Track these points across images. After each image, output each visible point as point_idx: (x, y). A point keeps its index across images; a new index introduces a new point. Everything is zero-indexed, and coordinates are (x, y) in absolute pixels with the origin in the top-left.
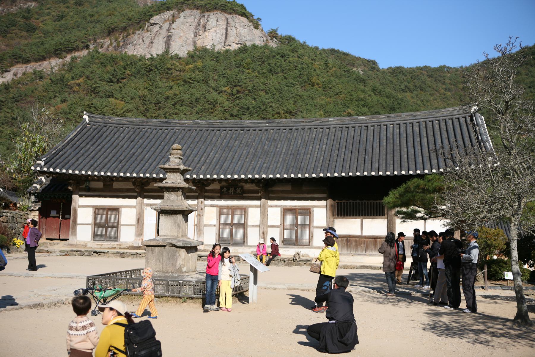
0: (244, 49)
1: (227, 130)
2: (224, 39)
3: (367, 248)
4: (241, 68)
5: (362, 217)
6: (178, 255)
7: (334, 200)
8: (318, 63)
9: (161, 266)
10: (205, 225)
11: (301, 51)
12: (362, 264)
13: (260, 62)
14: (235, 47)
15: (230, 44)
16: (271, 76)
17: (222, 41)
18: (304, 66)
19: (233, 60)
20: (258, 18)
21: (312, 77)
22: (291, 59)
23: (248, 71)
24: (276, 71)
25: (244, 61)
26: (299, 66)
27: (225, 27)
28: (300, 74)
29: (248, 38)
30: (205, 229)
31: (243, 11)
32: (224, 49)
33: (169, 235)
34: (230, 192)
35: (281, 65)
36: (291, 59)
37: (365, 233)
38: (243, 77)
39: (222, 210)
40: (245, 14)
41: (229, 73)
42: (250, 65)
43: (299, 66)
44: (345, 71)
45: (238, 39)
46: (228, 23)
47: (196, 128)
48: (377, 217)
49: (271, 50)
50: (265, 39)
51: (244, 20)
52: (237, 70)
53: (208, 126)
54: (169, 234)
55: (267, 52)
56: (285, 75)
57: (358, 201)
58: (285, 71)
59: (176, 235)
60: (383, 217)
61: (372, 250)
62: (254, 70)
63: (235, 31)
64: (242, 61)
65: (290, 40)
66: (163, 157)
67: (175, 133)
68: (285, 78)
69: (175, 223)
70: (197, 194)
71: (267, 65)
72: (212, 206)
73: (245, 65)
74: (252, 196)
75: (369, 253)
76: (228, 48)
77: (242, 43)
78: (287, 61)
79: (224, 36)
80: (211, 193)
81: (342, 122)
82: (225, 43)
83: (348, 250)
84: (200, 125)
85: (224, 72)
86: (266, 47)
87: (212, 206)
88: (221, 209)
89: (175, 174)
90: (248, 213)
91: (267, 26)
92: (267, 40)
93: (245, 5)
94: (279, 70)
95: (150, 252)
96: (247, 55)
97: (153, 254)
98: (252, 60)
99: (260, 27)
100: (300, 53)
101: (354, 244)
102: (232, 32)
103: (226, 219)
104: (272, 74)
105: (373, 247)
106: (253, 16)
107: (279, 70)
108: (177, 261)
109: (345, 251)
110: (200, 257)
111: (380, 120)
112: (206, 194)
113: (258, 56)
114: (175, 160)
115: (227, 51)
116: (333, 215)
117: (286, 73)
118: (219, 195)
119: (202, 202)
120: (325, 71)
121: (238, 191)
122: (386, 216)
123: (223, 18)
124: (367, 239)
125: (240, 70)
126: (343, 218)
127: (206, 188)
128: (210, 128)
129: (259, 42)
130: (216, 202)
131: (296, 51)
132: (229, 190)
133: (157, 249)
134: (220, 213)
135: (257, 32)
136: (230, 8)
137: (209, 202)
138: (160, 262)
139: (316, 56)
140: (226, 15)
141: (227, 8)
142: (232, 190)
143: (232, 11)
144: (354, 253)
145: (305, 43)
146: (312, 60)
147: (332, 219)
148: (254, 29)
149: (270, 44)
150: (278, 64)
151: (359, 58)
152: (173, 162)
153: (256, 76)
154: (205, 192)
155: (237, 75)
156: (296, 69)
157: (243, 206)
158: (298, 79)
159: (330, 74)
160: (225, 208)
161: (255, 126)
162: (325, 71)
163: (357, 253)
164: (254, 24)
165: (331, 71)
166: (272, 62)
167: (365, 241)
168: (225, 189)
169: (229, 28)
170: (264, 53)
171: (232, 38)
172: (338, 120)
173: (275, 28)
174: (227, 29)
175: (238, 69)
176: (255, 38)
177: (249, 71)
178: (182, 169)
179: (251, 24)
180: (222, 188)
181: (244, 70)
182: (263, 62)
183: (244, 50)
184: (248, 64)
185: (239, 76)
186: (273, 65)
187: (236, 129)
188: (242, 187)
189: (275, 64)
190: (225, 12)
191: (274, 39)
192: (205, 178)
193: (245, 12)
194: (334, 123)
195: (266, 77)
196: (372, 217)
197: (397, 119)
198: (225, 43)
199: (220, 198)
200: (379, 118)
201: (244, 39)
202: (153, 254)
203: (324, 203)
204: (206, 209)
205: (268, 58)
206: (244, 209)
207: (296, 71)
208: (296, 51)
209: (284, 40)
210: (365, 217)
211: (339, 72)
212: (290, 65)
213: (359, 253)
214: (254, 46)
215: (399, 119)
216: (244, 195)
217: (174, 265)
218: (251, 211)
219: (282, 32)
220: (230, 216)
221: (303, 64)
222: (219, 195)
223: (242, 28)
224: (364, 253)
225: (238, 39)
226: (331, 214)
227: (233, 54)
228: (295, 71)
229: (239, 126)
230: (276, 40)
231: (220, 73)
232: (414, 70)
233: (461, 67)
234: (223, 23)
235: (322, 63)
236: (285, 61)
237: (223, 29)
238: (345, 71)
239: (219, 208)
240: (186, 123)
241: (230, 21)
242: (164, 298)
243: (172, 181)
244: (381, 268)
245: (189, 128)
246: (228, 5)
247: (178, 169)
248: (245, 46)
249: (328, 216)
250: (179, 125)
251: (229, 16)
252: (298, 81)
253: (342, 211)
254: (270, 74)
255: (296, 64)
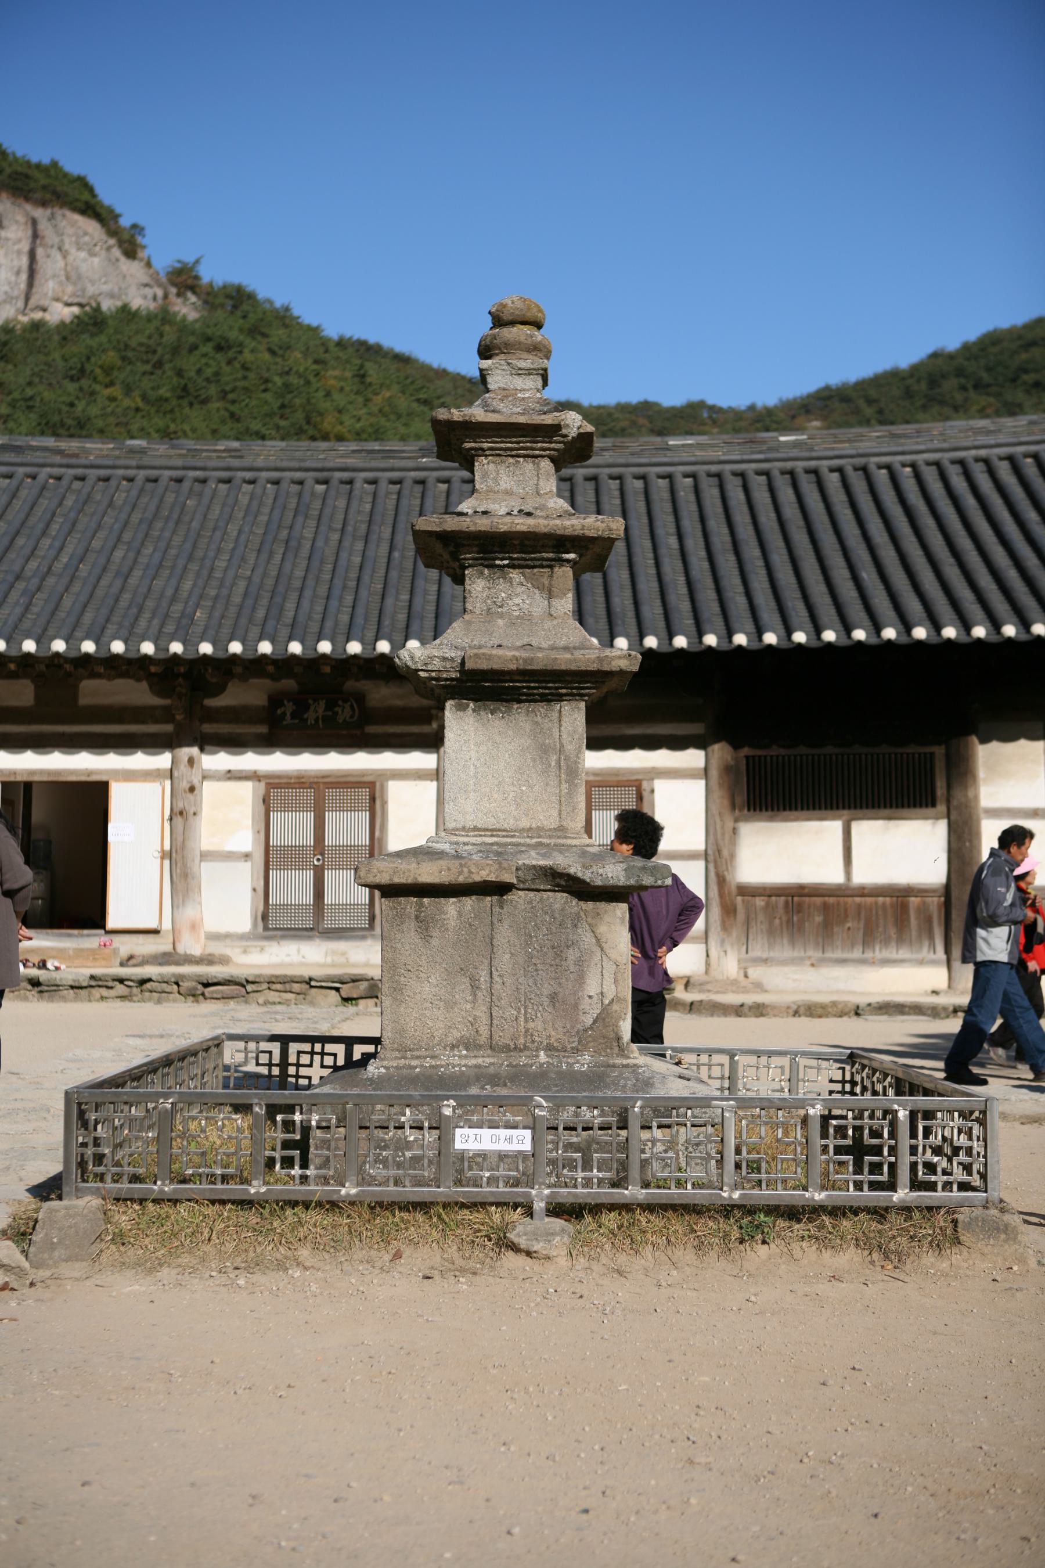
0: (92, 321)
1: (261, 482)
2: (23, 286)
3: (869, 936)
4: (85, 383)
5: (846, 813)
6: (588, 939)
7: (736, 746)
8: (337, 373)
9: (481, 1012)
10: (205, 856)
11: (278, 335)
12: (880, 999)
13: (147, 362)
14: (60, 313)
15: (45, 302)
16: (187, 410)
17: (16, 293)
18: (294, 380)
19: (57, 355)
20: (134, 226)
21: (321, 414)
22: (247, 356)
23: (107, 392)
24: (203, 394)
25: (93, 360)
26: (278, 380)
27: (25, 246)
28: (283, 406)
29: (105, 288)
30: (207, 872)
31: (86, 196)
32: (24, 319)
33: (510, 823)
34: (310, 716)
35: (217, 374)
36: (247, 356)
37: (864, 875)
38: (94, 411)
39: (275, 792)
40: (91, 208)
41: (47, 395)
42: (115, 373)
43: (278, 380)
44: (418, 400)
45: (70, 289)
46: (35, 236)
47: (131, 473)
48: (905, 812)
49: (183, 327)
50: (160, 293)
51: (92, 227)
52: (71, 387)
53: (179, 463)
54: (509, 816)
55: (170, 335)
56: (232, 408)
57: (829, 750)
58: (231, 396)
59: (552, 823)
60: (930, 811)
61: (886, 942)
62: (128, 390)
63: (61, 263)
64: (88, 358)
65: (238, 298)
66: (18, 577)
67: (44, 488)
68: (232, 415)
69: (544, 750)
70: (169, 728)
71: (170, 373)
72: (231, 776)
73: (98, 371)
74: (401, 735)
75: (879, 953)
76: (38, 315)
77: (83, 301)
78: (237, 365)
79: (24, 276)
80: (229, 721)
81: (719, 454)
82: (27, 299)
83: (793, 942)
84: (146, 461)
85: (29, 392)
86: (164, 316)
87: (231, 776)
88: (270, 786)
89: (528, 466)
90: (384, 803)
91: (164, 251)
92: (166, 296)
93: (92, 180)
94: (213, 390)
95: (411, 925)
96: (103, 338)
97: (426, 937)
98: (124, 359)
99: (142, 254)
100: (275, 339)
101: (818, 919)
102: (51, 264)
103: (294, 827)
104: (191, 405)
105: (892, 931)
106: (116, 217)
107: (213, 390)
108: (581, 978)
109: (784, 950)
110: (206, 985)
111: (865, 446)
112: (208, 728)
113: (141, 344)
114: (519, 382)
115: (37, 326)
116: (733, 806)
117: (233, 402)
118: (263, 729)
119: (191, 761)
120: (360, 399)
121: (344, 712)
122: (941, 808)
123: (21, 218)
124: (869, 900)
125: (81, 389)
126: (771, 819)
127: (209, 702)
128: (192, 474)
129: (139, 300)
130: (251, 761)
131: (265, 335)
132: (307, 708)
133: (451, 907)
134: (267, 804)
135: (134, 269)
136: (44, 187)
137: (220, 760)
138: (475, 987)
139: (326, 351)
140: (28, 207)
141: (32, 185)
142: (317, 710)
143: (48, 196)
144: (819, 954)
145: (287, 309)
146: (316, 362)
147: (730, 824)
148: (123, 259)
149: (176, 309)
150: (209, 372)
151: (442, 373)
152: (507, 394)
153: (137, 410)
154: (203, 720)
155: (72, 405)
156: (265, 390)
157: (364, 773)
158: (277, 419)
159: (375, 409)
160: (288, 785)
161: (374, 464)
162: (360, 399)
163: (829, 954)
164: (120, 243)
165: (378, 400)
166: (190, 364)
167: (859, 906)
168: (289, 708)
169: (40, 252)
170: (161, 336)
171: (51, 284)
172: (700, 446)
173: (190, 259)
174: (32, 255)
175: (76, 385)
176: (127, 287)
177: (116, 391)
178: (573, 433)
179: (112, 241)
180: (275, 700)
181: (97, 387)
182: (159, 365)
183: (95, 324)
184: (108, 370)
185: (80, 406)
186: (192, 374)
187: (298, 475)
188: (360, 698)
189: (199, 372)
190: (27, 199)
191: (189, 294)
192: (221, 655)
193: (93, 201)
194: (685, 457)
195: (172, 411)
196: (887, 812)
197: (930, 446)
198: (27, 299)
199: (267, 743)
200: (860, 438)
201: (91, 290)
202: (426, 937)
203: (694, 758)
204: (209, 790)
205: (175, 351)
206: (371, 786)
207: (268, 396)
208: (265, 335)
209: (221, 300)
210: (859, 812)
211: (403, 403)
212: (245, 378)
213: (839, 954)
214: (126, 313)
215: (936, 444)
216: (371, 729)
217: (563, 1003)
218: (396, 792)
219: (214, 273)
220: (311, 816)
221: (288, 373)
222: (263, 729)
223: (83, 254)
224: (857, 953)
225: (70, 289)
226: (726, 802)
227: (56, 338)
228: (263, 395)
229: (308, 464)
230: (193, 298)
231: (16, 395)
232: (610, 415)
233: (752, 408)
234: (20, 234)
235: (348, 374)
236: (229, 362)
237: (19, 252)
238: (418, 400)
239: (262, 786)
240: (88, 452)
241: (44, 226)
242: (610, 1220)
243: (516, 505)
244: (955, 1011)
245: (103, 472)
246: (37, 174)
247: (554, 430)
248: (98, 309)
249: (714, 809)
250: (58, 459)
251: (39, 213)
252: (278, 428)
253: (765, 789)
254: (185, 402)
255: (266, 375)
